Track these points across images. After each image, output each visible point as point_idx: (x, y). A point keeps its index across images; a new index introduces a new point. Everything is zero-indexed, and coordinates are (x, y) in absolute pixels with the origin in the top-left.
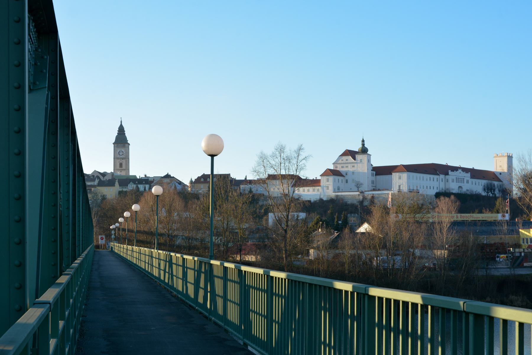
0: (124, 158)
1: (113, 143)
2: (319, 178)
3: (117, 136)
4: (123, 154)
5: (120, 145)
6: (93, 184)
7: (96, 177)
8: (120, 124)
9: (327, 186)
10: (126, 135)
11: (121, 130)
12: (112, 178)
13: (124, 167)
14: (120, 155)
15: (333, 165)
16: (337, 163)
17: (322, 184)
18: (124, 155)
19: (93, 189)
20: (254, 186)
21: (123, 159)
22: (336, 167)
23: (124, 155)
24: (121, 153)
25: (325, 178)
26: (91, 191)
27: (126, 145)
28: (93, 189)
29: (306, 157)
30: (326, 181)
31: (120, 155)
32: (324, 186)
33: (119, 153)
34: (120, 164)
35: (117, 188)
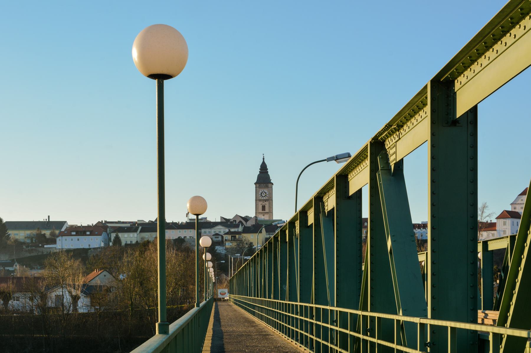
0: (267, 200)
1: (255, 183)
2: (494, 221)
3: (259, 174)
4: (265, 196)
5: (263, 185)
6: (237, 231)
7: (239, 222)
8: (262, 162)
9: (504, 230)
10: (269, 173)
11: (264, 168)
12: (255, 223)
13: (267, 210)
14: (263, 196)
15: (510, 206)
16: (516, 204)
17: (497, 228)
18: (267, 196)
19: (237, 236)
20: (418, 231)
21: (266, 200)
22: (515, 208)
23: (267, 196)
24: (264, 194)
25: (502, 221)
26: (236, 238)
27: (270, 185)
28: (237, 236)
29: (489, 214)
30: (503, 225)
31: (262, 196)
32: (500, 230)
33: (261, 193)
34: (263, 206)
35: (263, 235)
